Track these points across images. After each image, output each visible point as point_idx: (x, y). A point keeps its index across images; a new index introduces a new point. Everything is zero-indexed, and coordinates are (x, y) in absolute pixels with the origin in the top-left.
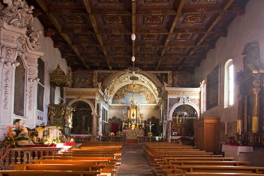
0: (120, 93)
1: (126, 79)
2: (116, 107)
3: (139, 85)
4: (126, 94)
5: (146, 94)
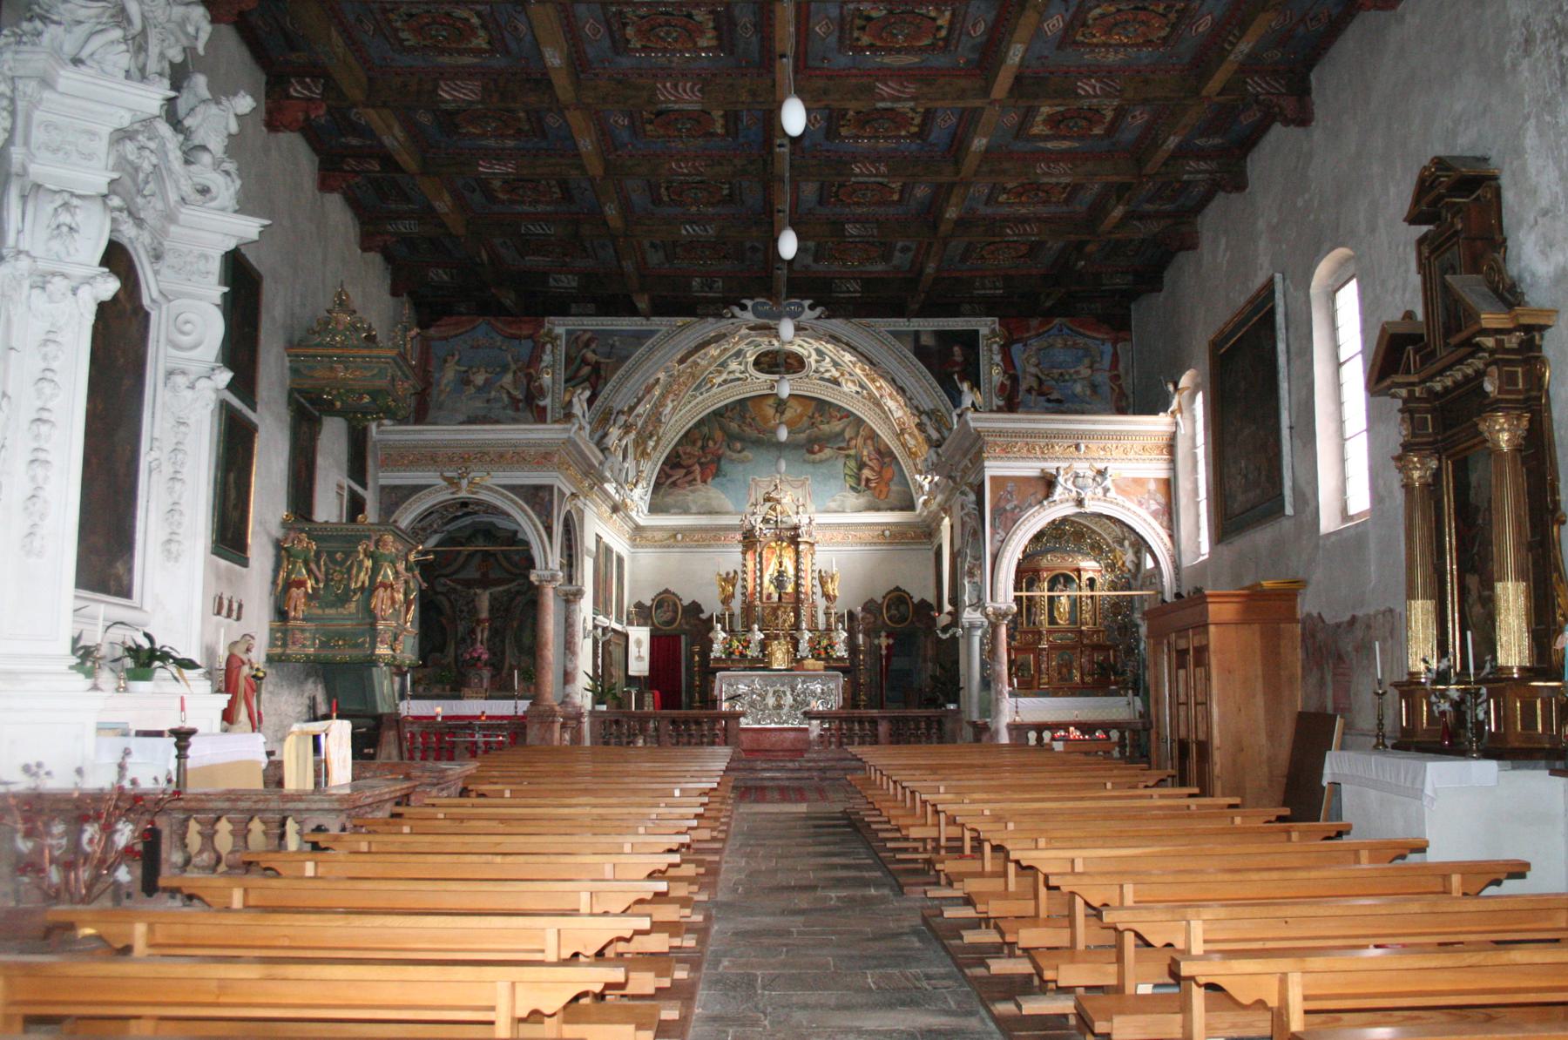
0: (696, 451)
1: (733, 366)
2: (674, 532)
3: (808, 402)
4: (735, 456)
5: (852, 452)
